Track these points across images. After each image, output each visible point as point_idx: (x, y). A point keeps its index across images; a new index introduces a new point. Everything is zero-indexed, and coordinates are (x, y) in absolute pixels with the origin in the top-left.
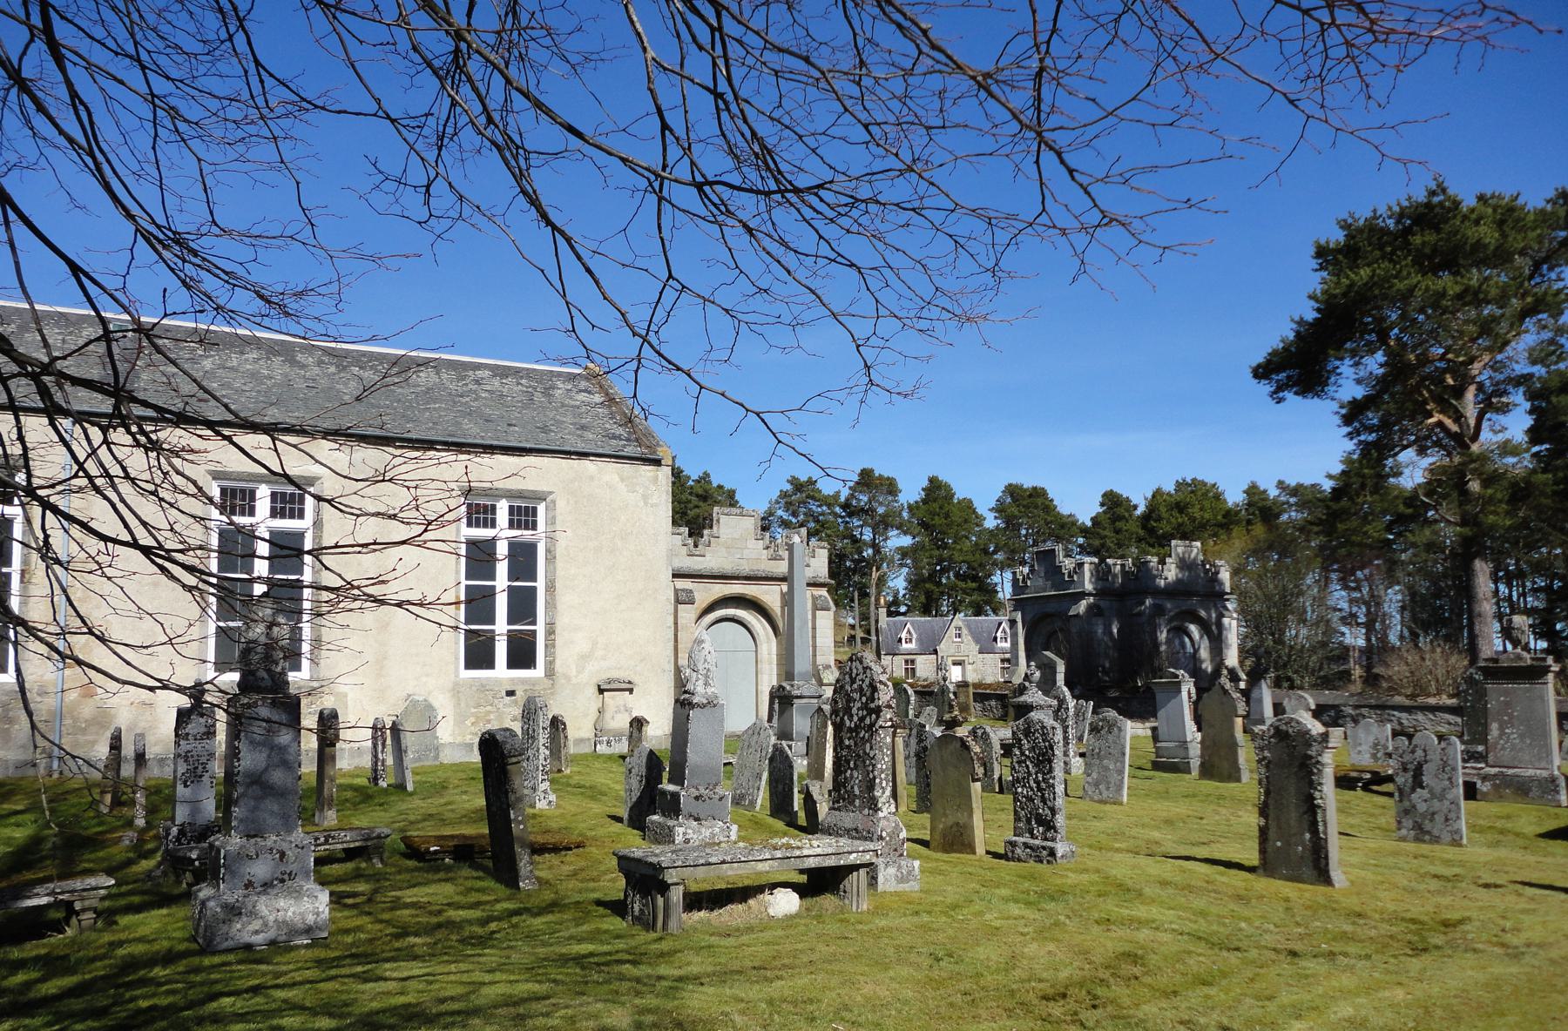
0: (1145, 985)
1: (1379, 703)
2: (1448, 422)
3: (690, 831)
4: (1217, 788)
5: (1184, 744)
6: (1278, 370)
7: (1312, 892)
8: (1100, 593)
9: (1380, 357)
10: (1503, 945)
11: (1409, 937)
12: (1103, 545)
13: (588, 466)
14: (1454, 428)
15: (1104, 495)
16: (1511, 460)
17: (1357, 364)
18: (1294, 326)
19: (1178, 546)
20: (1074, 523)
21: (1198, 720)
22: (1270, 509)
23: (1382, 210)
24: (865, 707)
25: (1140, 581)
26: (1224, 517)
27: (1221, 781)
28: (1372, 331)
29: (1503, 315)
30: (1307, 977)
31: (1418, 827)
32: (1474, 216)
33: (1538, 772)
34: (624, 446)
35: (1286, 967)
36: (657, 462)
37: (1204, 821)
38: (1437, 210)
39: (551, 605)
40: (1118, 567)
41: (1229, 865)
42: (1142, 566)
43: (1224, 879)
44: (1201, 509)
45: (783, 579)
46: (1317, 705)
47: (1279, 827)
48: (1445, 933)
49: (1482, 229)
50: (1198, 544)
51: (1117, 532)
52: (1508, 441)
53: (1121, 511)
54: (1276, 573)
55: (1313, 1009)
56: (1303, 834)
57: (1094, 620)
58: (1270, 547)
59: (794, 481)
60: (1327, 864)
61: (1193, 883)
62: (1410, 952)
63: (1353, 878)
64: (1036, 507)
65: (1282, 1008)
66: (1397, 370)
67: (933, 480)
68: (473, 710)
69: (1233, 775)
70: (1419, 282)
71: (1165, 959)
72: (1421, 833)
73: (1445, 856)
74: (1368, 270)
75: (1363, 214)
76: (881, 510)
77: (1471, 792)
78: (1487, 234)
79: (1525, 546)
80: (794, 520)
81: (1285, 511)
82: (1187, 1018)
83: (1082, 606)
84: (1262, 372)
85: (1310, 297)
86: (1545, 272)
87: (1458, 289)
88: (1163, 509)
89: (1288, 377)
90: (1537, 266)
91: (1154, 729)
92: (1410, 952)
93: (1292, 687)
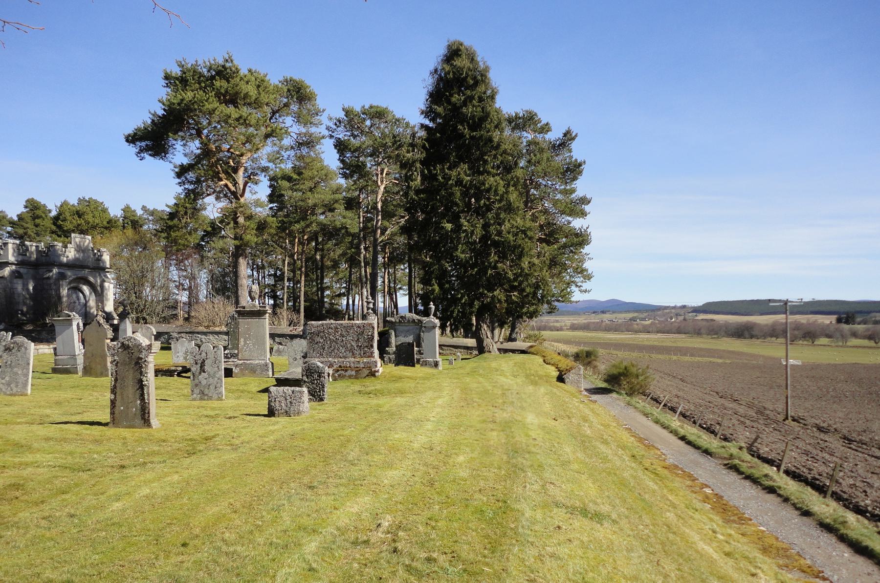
0: (22, 501)
1: (191, 330)
2: (230, 185)
4: (94, 381)
5: (74, 356)
6: (141, 139)
7: (143, 432)
8: (20, 264)
9: (197, 143)
10: (232, 445)
11: (188, 448)
12: (26, 234)
14: (233, 189)
15: (27, 201)
16: (259, 209)
17: (184, 145)
18: (151, 116)
19: (76, 238)
20: (4, 217)
21: (83, 341)
22: (137, 222)
23: (200, 62)
25: (47, 259)
26: (108, 223)
27: (97, 377)
28: (194, 128)
29: (257, 134)
30: (127, 478)
32: (246, 79)
33: (260, 361)
35: (116, 475)
37: (82, 401)
38: (228, 70)
40: (34, 248)
41: (92, 423)
42: (50, 247)
43: (88, 432)
46: (157, 333)
47: (122, 398)
48: (205, 444)
49: (249, 87)
50: (90, 237)
51: (37, 226)
52: (258, 200)
53: (38, 212)
54: (138, 258)
55: (127, 494)
56: (136, 401)
57: (15, 281)
58: (136, 244)
60: (149, 416)
61: (67, 436)
62: (186, 456)
63: (163, 422)
65: (110, 497)
66: (206, 153)
69: (103, 374)
70: (218, 107)
71: (39, 483)
72: (203, 396)
73: (213, 405)
74: (192, 94)
75: (190, 63)
77: (228, 373)
78: (252, 91)
79: (266, 253)
81: (146, 223)
82: (48, 514)
83: (7, 271)
85: (159, 101)
86: (277, 117)
87: (237, 116)
88: (67, 214)
89: (147, 145)
90: (274, 113)
91: (55, 349)
92: (186, 456)
93: (146, 323)
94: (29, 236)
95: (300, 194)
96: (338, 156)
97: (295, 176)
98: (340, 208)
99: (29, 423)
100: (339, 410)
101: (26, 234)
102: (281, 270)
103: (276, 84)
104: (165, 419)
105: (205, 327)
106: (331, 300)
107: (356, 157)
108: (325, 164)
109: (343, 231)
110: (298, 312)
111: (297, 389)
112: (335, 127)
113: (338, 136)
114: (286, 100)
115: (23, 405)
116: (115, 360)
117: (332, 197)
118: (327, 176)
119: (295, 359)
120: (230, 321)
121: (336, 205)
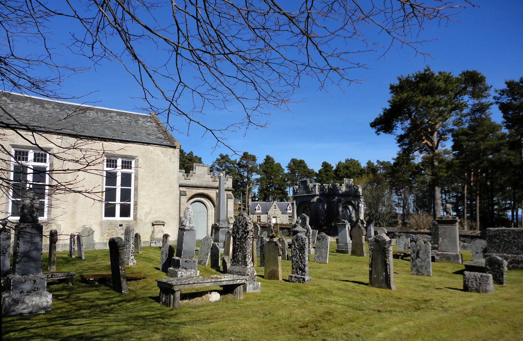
2: (429, 143)
3: (183, 273)
5: (346, 244)
6: (378, 125)
8: (321, 195)
9: (409, 121)
11: (414, 305)
12: (322, 179)
13: (150, 148)
14: (431, 145)
15: (323, 163)
16: (447, 156)
17: (402, 123)
18: (383, 111)
19: (346, 180)
20: (313, 172)
22: (375, 169)
24: (244, 231)
25: (334, 191)
26: (360, 171)
27: (358, 256)
30: (383, 318)
31: (418, 270)
32: (438, 79)
34: (163, 141)
35: (377, 315)
36: (175, 147)
37: (352, 269)
39: (136, 195)
41: (360, 283)
42: (334, 186)
43: (358, 288)
44: (353, 169)
45: (217, 188)
48: (425, 304)
49: (440, 83)
51: (327, 175)
52: (446, 150)
53: (328, 168)
54: (376, 189)
55: (385, 329)
56: (383, 273)
58: (374, 181)
59: (221, 156)
60: (390, 282)
64: (301, 166)
65: (376, 328)
66: (414, 126)
67: (268, 157)
68: (108, 231)
72: (418, 272)
75: (405, 76)
76: (250, 166)
77: (433, 259)
79: (451, 183)
80: (221, 169)
81: (379, 170)
83: (315, 199)
84: (373, 125)
85: (388, 102)
87: (433, 101)
88: (341, 168)
89: (381, 127)
90: (456, 95)
91: (337, 239)
92: (415, 310)
93: (380, 226)
94: (324, 181)
95: (474, 143)
96: (502, 115)
97: (471, 132)
98: (505, 150)
99: (329, 279)
100: (517, 292)
101: (322, 179)
102: (461, 193)
103: (457, 77)
104: (398, 284)
105: (415, 229)
106: (499, 212)
107: (517, 113)
108: (492, 121)
109: (508, 164)
110: (475, 220)
111: (484, 274)
112: (499, 96)
113: (502, 101)
114: (464, 85)
115: (325, 269)
116: (371, 249)
117: (498, 142)
118: (494, 128)
119: (477, 253)
120: (432, 226)
121: (502, 148)
